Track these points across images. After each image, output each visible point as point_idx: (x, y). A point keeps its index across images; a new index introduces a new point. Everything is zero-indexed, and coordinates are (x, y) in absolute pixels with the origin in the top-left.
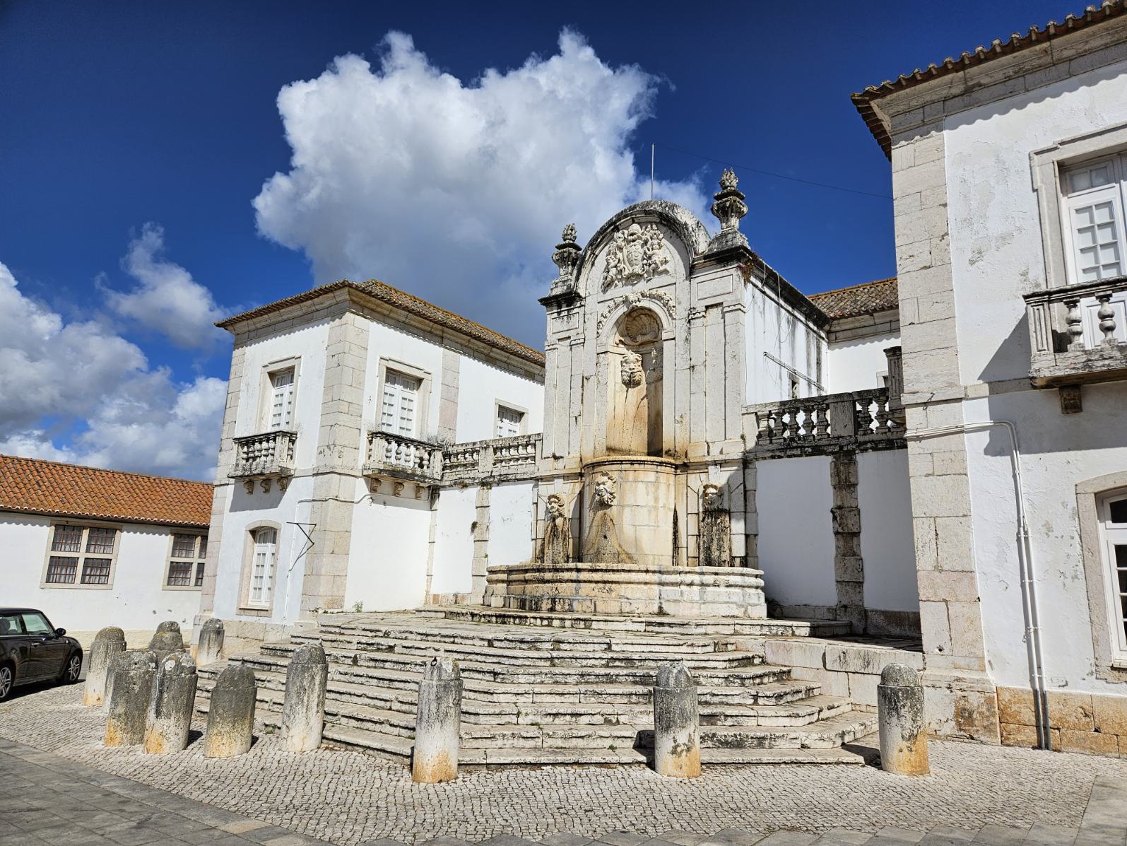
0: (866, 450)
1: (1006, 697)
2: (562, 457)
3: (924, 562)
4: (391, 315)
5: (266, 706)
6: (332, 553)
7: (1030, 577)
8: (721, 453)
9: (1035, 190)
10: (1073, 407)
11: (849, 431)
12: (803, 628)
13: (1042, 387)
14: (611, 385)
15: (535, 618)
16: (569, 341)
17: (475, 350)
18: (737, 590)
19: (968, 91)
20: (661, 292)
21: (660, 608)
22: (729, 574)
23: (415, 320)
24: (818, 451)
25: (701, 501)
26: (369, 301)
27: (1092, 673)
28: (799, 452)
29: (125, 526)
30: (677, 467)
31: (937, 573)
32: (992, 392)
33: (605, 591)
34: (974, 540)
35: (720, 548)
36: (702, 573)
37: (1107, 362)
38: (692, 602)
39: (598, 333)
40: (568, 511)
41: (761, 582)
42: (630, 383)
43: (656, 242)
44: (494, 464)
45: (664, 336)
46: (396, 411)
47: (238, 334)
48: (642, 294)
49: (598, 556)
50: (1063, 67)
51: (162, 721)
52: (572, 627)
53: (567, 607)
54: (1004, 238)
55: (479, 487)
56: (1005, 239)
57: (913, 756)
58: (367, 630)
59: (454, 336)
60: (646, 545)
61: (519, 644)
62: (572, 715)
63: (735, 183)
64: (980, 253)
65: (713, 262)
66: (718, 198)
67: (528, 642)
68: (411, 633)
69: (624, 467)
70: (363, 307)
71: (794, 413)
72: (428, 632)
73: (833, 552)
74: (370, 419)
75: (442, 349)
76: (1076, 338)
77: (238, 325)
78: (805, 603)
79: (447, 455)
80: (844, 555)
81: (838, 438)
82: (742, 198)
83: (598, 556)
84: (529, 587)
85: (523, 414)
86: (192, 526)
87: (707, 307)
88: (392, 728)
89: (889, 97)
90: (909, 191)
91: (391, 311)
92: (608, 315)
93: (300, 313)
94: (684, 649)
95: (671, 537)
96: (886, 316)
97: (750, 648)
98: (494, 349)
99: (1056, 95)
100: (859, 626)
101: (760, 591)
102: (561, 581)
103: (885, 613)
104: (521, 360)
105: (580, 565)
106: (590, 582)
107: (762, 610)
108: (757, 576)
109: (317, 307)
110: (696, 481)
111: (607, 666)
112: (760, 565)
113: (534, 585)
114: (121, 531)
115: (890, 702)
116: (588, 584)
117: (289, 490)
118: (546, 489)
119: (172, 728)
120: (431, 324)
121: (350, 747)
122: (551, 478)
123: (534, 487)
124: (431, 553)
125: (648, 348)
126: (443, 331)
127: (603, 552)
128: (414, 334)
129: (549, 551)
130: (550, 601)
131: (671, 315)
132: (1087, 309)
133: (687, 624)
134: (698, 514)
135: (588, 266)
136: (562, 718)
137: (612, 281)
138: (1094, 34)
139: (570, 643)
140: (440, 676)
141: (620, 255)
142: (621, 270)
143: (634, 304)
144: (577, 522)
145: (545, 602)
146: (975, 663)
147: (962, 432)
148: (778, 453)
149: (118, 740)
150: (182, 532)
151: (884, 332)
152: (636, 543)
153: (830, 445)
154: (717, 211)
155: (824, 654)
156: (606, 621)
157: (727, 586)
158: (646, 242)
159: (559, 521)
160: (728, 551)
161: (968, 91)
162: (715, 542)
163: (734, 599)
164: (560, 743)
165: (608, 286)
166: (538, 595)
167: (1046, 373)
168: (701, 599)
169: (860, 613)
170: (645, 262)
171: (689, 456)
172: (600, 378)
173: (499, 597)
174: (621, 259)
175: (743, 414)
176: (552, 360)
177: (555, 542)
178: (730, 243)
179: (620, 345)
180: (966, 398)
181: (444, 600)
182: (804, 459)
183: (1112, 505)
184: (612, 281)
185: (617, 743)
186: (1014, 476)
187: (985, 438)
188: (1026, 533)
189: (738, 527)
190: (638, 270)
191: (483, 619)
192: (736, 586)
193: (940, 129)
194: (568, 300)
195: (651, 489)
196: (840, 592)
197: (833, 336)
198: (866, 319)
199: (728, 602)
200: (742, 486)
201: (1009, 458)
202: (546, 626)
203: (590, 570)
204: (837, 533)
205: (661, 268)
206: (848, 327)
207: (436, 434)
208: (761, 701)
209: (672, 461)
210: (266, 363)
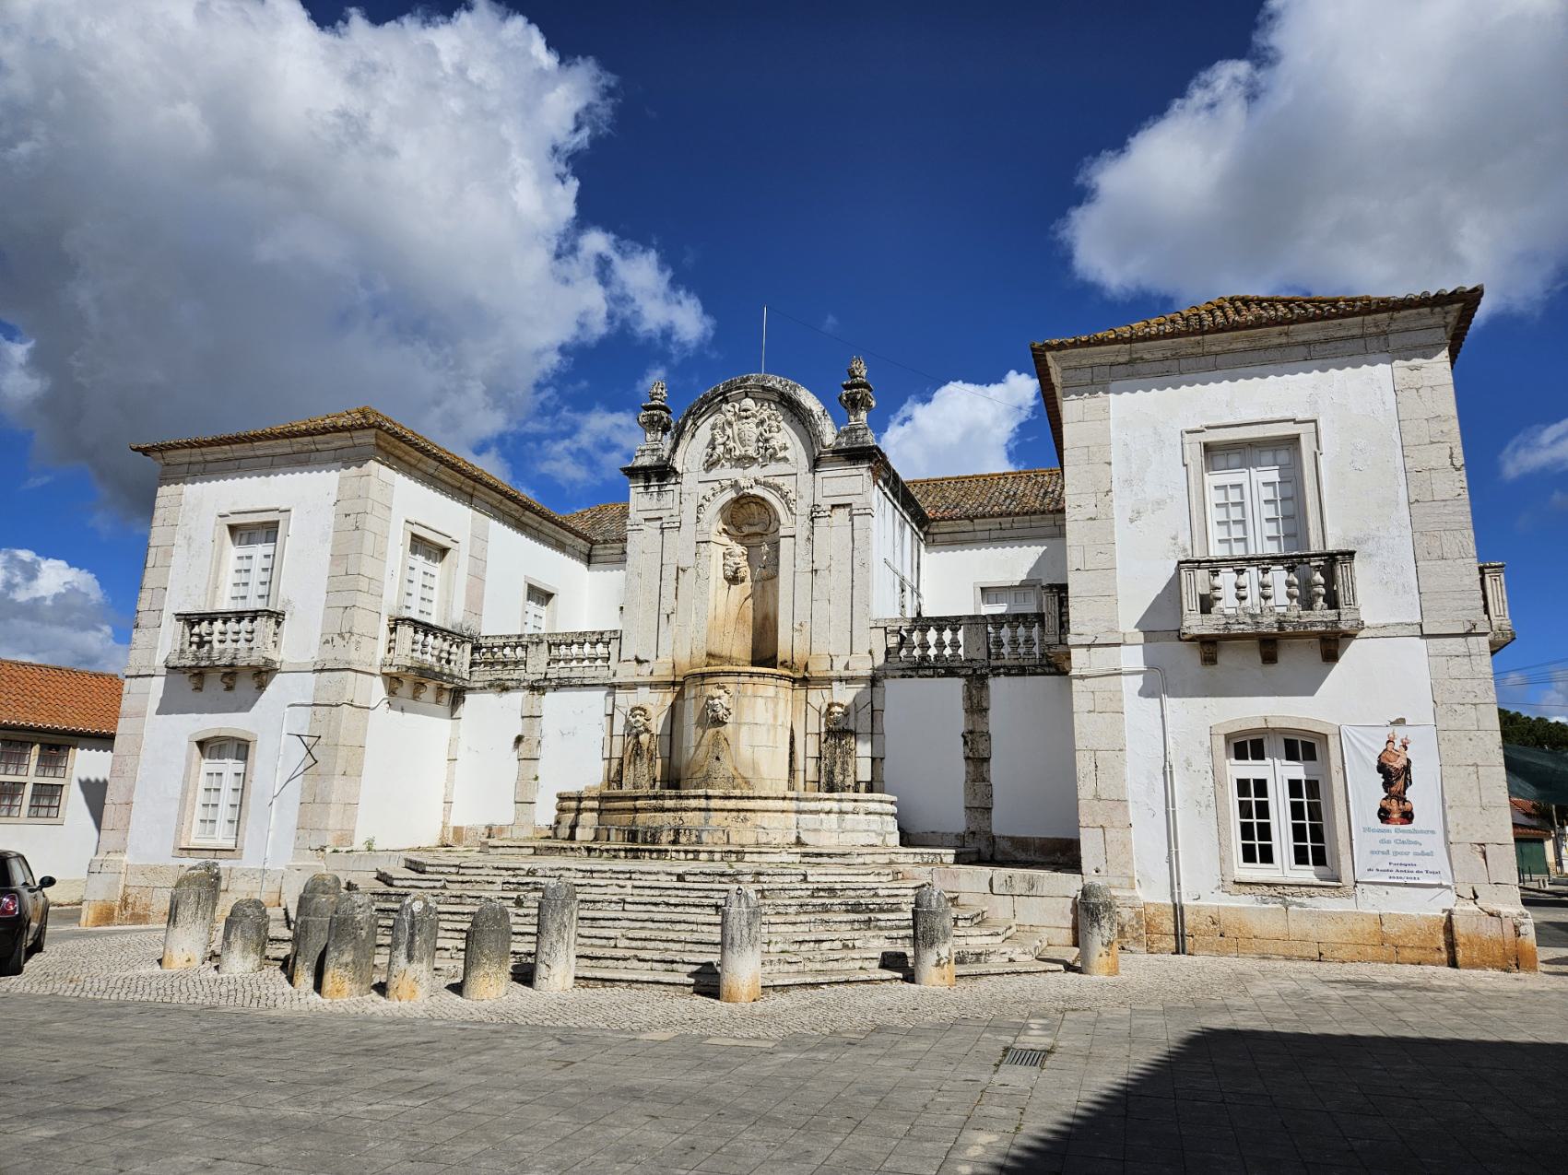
0: (998, 675)
1: (1151, 910)
2: (647, 661)
3: (1085, 792)
4: (420, 465)
5: (447, 954)
6: (344, 774)
7: (1173, 806)
8: (847, 667)
9: (1185, 465)
10: (1210, 660)
11: (982, 655)
12: (949, 855)
13: (1187, 640)
14: (712, 579)
15: (678, 851)
16: (659, 522)
17: (504, 513)
18: (876, 817)
19: (1131, 362)
20: (779, 481)
21: (798, 838)
22: (869, 801)
23: (446, 474)
24: (951, 672)
25: (823, 720)
26: (396, 447)
27: (1219, 888)
29: (82, 741)
30: (794, 681)
31: (1096, 802)
32: (1146, 640)
34: (1128, 772)
35: (844, 771)
37: (1242, 626)
38: (830, 831)
40: (657, 724)
41: (893, 809)
42: (734, 579)
43: (774, 424)
44: (549, 664)
45: (782, 532)
46: (416, 589)
47: (168, 465)
48: (756, 481)
49: (707, 780)
50: (1211, 359)
51: (415, 965)
53: (694, 839)
54: (1159, 504)
55: (527, 692)
56: (1159, 504)
57: (1110, 959)
58: (502, 869)
59: (485, 494)
60: (764, 770)
62: (816, 941)
63: (864, 374)
64: (1139, 513)
65: (842, 458)
66: (846, 387)
67: (729, 875)
68: (569, 870)
69: (741, 679)
70: (389, 454)
71: (924, 630)
72: (594, 869)
73: (963, 777)
74: (391, 603)
75: (471, 510)
76: (1218, 602)
77: (170, 453)
79: (476, 649)
80: (974, 781)
81: (972, 660)
82: (871, 390)
83: (707, 780)
84: (641, 817)
85: (552, 595)
86: (31, 729)
87: (833, 506)
88: (642, 964)
89: (1063, 352)
90: (1079, 444)
91: (420, 460)
92: (712, 498)
93: (288, 450)
94: (871, 878)
95: (787, 759)
96: (986, 524)
97: (916, 876)
98: (527, 512)
99: (1205, 383)
100: (987, 852)
102: (685, 810)
103: (1011, 839)
104: (554, 526)
105: (710, 792)
107: (894, 839)
108: (892, 803)
109: (318, 447)
110: (818, 698)
111: (813, 897)
112: (887, 789)
113: (649, 815)
114: (75, 748)
115: (1092, 915)
116: (719, 813)
117: (270, 688)
118: (625, 700)
119: (425, 973)
120: (463, 478)
121: (608, 984)
122: (633, 686)
123: (608, 694)
124: (451, 774)
125: (756, 540)
126: (474, 489)
127: (714, 775)
128: (442, 491)
129: (629, 774)
131: (790, 509)
132: (1227, 578)
134: (820, 734)
135: (688, 436)
136: (807, 945)
137: (719, 460)
138: (1237, 338)
140: (748, 903)
141: (729, 431)
143: (746, 490)
144: (667, 740)
145: (665, 834)
146: (1126, 882)
147: (1120, 674)
148: (909, 673)
149: (347, 990)
150: (12, 737)
151: (983, 540)
153: (963, 667)
154: (846, 402)
155: (991, 879)
156: (760, 853)
158: (762, 422)
159: (644, 738)
160: (853, 776)
161: (1131, 362)
162: (839, 764)
163: (874, 827)
164: (818, 966)
167: (1195, 631)
169: (988, 839)
170: (761, 444)
171: (809, 669)
173: (587, 829)
176: (635, 543)
177: (638, 762)
178: (860, 440)
180: (1124, 644)
181: (471, 833)
182: (936, 680)
183: (1235, 744)
184: (719, 460)
185: (866, 964)
186: (1163, 716)
187: (1139, 680)
188: (1171, 767)
189: (864, 749)
190: (751, 452)
191: (605, 854)
192: (876, 813)
193: (1107, 392)
194: (662, 473)
195: (770, 705)
196: (969, 819)
197: (930, 538)
198: (966, 525)
200: (870, 706)
201: (1158, 700)
203: (721, 798)
204: (967, 758)
205: (780, 455)
206: (946, 530)
207: (460, 620)
208: (960, 923)
209: (791, 674)
210: (225, 512)
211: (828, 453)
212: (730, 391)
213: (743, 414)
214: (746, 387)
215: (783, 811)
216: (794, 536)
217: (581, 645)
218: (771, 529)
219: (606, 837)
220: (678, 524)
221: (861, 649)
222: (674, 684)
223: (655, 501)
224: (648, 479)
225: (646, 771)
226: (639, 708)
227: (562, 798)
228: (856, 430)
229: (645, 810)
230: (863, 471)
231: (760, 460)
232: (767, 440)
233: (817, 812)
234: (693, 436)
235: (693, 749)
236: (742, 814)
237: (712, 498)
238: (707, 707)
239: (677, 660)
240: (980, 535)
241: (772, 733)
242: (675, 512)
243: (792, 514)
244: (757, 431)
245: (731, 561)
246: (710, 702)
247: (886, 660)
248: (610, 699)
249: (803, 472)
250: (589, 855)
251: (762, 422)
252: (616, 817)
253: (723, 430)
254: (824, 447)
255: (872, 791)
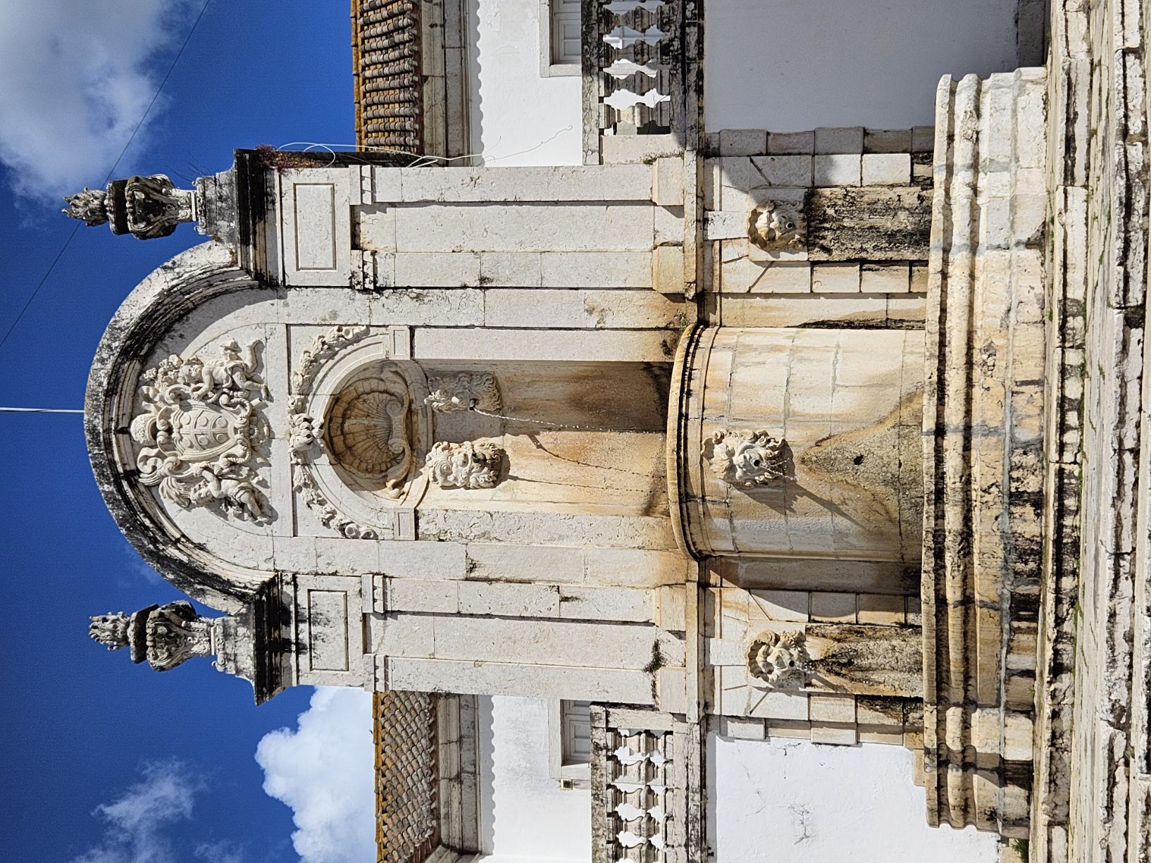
2: (656, 646)
8: (678, 211)
15: (1062, 447)
16: (373, 621)
20: (299, 363)
21: (1029, 244)
25: (785, 256)
28: (692, 32)
30: (703, 323)
33: (990, 361)
35: (890, 209)
36: (950, 169)
39: (367, 537)
42: (498, 468)
45: (402, 354)
52: (1081, 347)
53: (1031, 459)
61: (1135, 218)
63: (98, 193)
66: (122, 228)
67: (1129, 188)
68: (1113, 615)
69: (694, 412)
78: (1011, 23)
84: (984, 588)
87: (355, 246)
92: (329, 507)
96: (432, 52)
101: (987, 83)
102: (967, 481)
105: (929, 424)
106: (968, 399)
113: (977, 569)
116: (975, 406)
122: (706, 671)
123: (723, 734)
125: (422, 425)
127: (894, 468)
129: (889, 682)
130: (1017, 510)
131: (357, 339)
133: (1068, 74)
134: (814, 264)
135: (201, 558)
137: (252, 491)
139: (1126, 116)
142: (233, 464)
143: (315, 432)
145: (1020, 527)
148: (692, 77)
151: (463, 60)
152: (881, 383)
154: (149, 223)
156: (1065, 266)
157: (979, 116)
158: (180, 398)
159: (815, 649)
160: (899, 190)
162: (877, 221)
163: (1007, 100)
165: (261, 507)
166: (1001, 554)
168: (1006, 168)
171: (680, 289)
172: (476, 531)
173: (1009, 733)
174: (204, 464)
175: (601, 162)
177: (865, 663)
179: (405, 489)
182: (708, 23)
190: (237, 420)
191: (1067, 627)
195: (751, 357)
199: (1014, 111)
202: (1080, 416)
205: (246, 358)
206: (441, 130)
211: (245, 256)
212: (112, 463)
213: (161, 437)
214: (107, 431)
215: (972, 276)
216: (412, 329)
217: (618, 796)
218: (398, 388)
219: (1026, 681)
220: (378, 581)
221: (642, 183)
222: (703, 585)
223: (327, 630)
224: (284, 645)
225: (885, 644)
226: (752, 657)
227: (939, 812)
228: (207, 202)
229: (967, 579)
230: (287, 183)
231: (255, 402)
232: (216, 387)
233: (974, 209)
234: (201, 547)
235: (839, 519)
236: (978, 357)
237: (329, 507)
238: (747, 486)
239: (656, 581)
240: (453, 67)
241: (804, 354)
242: (352, 585)
243: (366, 333)
244: (197, 406)
245: (459, 472)
246: (739, 473)
247: (666, 130)
248: (733, 728)
249: (284, 311)
250: (1070, 670)
251: (180, 398)
252: (981, 657)
253: (192, 480)
254: (234, 263)
255: (930, 153)
